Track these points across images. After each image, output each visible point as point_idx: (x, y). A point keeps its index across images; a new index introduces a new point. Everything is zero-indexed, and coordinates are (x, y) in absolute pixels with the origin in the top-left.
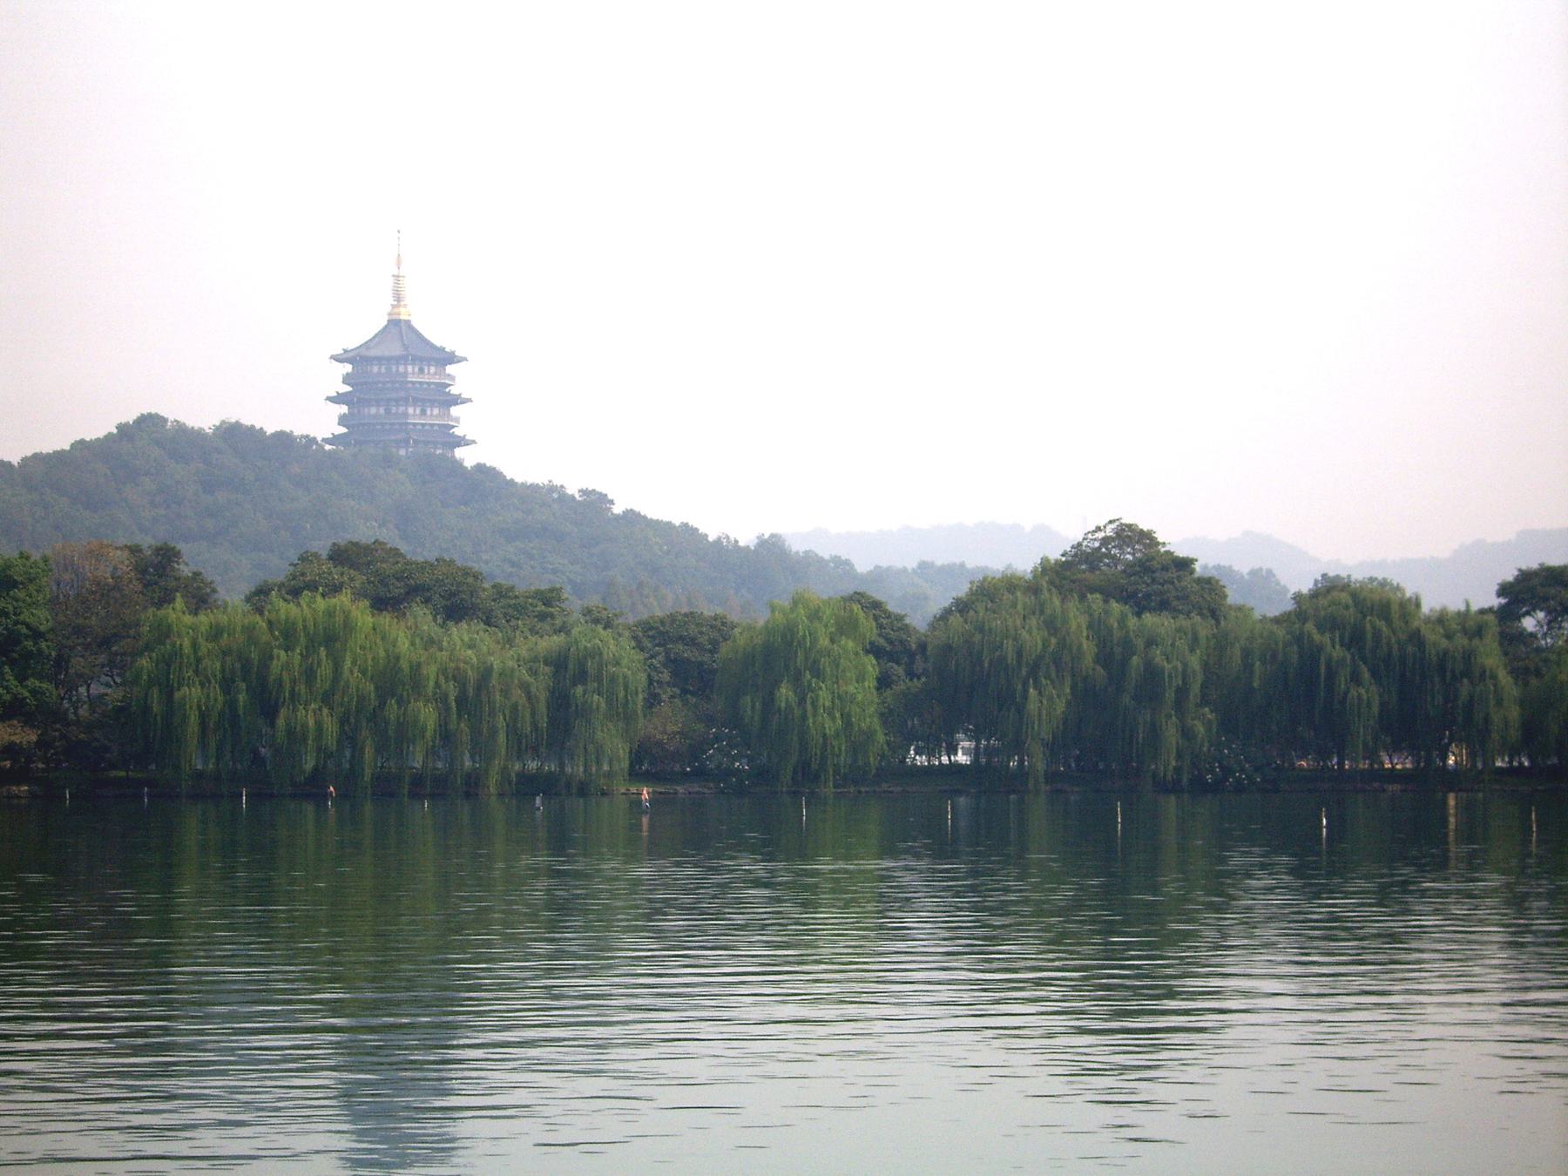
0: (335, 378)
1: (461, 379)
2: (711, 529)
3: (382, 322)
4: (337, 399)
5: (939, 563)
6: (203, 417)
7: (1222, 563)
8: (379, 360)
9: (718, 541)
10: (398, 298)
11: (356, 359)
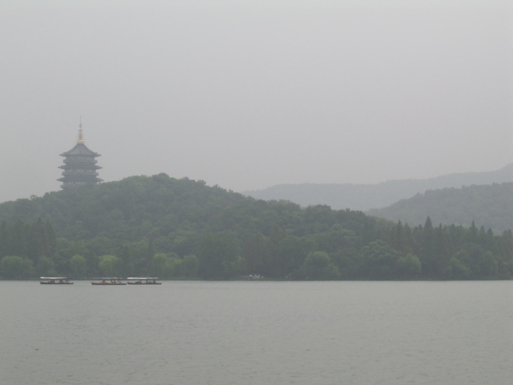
0: (61, 161)
1: (100, 161)
2: (171, 176)
3: (75, 144)
4: (61, 180)
5: (304, 204)
6: (41, 194)
7: (263, 199)
9: (198, 181)
10: (81, 137)
11: (66, 155)
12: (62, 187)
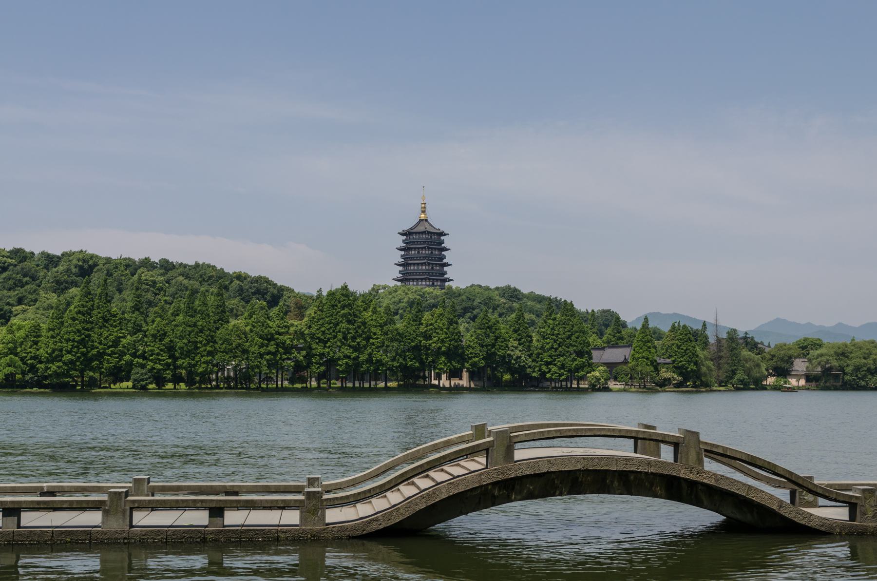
1: (447, 242)
8: (416, 233)
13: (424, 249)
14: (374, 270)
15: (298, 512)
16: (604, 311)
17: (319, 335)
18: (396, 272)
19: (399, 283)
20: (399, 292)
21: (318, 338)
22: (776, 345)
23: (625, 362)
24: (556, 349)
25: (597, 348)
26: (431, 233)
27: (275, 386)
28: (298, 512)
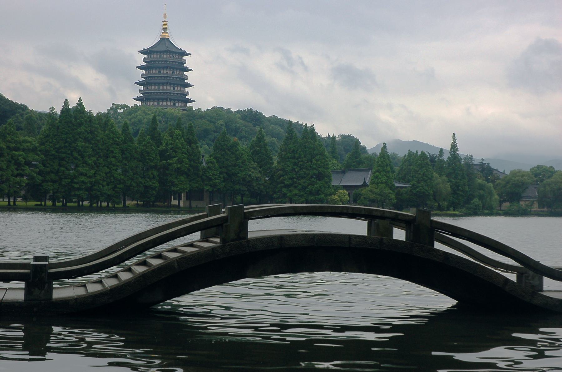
0: (140, 59)
1: (189, 62)
8: (157, 52)
12: (140, 92)
13: (165, 66)
14: (104, 87)
15: (366, 223)
16: (343, 137)
17: (53, 152)
18: (137, 92)
19: (139, 103)
20: (140, 112)
21: (53, 155)
22: (511, 172)
23: (365, 185)
24: (297, 172)
25: (335, 171)
26: (173, 52)
27: (177, 204)
28: (366, 223)
